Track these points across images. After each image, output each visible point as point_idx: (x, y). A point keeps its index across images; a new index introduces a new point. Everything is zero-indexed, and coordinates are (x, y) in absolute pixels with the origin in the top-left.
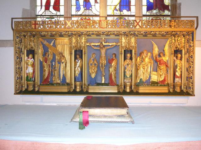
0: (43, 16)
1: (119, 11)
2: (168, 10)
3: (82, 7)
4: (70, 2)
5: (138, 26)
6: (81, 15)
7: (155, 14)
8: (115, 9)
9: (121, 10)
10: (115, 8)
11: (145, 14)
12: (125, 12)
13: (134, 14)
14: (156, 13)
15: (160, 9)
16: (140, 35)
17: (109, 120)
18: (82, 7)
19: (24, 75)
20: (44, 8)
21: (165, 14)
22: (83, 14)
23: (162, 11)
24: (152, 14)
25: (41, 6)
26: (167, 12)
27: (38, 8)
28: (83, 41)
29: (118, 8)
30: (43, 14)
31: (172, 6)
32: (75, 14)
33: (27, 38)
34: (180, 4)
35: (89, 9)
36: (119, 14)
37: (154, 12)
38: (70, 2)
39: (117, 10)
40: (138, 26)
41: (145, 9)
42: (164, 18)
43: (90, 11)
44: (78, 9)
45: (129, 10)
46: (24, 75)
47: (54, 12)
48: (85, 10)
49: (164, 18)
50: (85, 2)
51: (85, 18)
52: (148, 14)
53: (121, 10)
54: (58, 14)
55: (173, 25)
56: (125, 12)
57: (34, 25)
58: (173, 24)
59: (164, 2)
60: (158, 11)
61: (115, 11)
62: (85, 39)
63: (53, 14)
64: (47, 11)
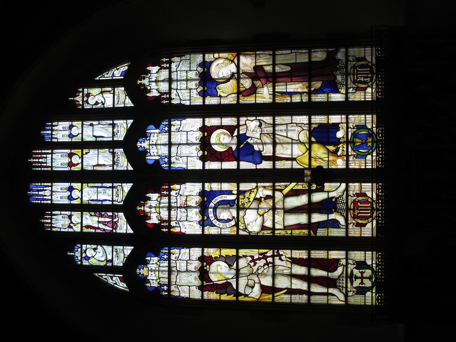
0: (347, 291)
1: (339, 146)
2: (336, 52)
6: (346, 220)
7: (344, 76)
8: (335, 153)
17: (300, 164)
19: (83, 208)
21: (344, 59)
22: (345, 214)
23: (338, 64)
24: (344, 83)
25: (327, 294)
26: (340, 55)
27: (334, 301)
29: (332, 148)
30: (344, 291)
32: (344, 230)
35: (335, 203)
39: (337, 150)
42: (352, 60)
43: (340, 201)
46: (83, 208)
48: (336, 211)
50: (322, 211)
51: (352, 211)
52: (343, 91)
54: (343, 262)
57: (50, 198)
59: (320, 60)
60: (338, 72)
61: (339, 154)
63: (344, 272)
64: (338, 284)
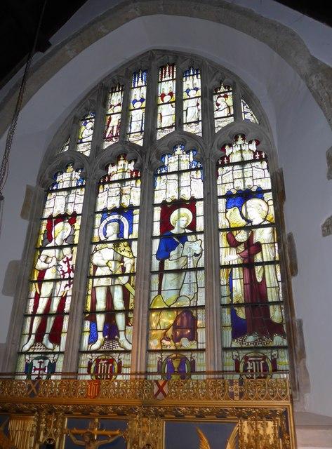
2: (281, 333)
3: (100, 336)
4: (216, 243)
5: (161, 394)
6: (96, 351)
7: (252, 345)
9: (176, 339)
10: (165, 334)
11: (228, 345)
12: (186, 344)
13: (203, 346)
14: (255, 342)
15: (262, 333)
16: (232, 415)
18: (100, 336)
20: (33, 337)
24: (244, 346)
26: (278, 340)
28: (270, 431)
29: (170, 333)
31: (288, 324)
33: (95, 178)
34: (300, 322)
36: (172, 348)
37: (250, 339)
38: (216, 243)
39: (168, 339)
40: (161, 394)
41: (228, 333)
42: (273, 354)
44: (93, 340)
45: (193, 337)
47: (50, 346)
49: (273, 354)
53: (176, 339)
55: (237, 392)
56: (186, 344)
58: (236, 389)
59: (271, 315)
61: (164, 341)
62: (275, 428)
63: (47, 351)
